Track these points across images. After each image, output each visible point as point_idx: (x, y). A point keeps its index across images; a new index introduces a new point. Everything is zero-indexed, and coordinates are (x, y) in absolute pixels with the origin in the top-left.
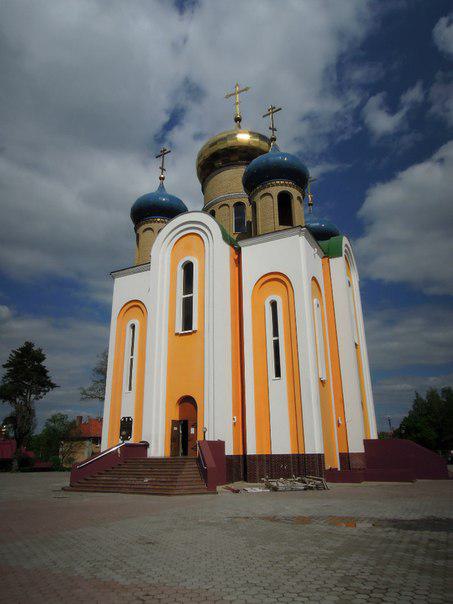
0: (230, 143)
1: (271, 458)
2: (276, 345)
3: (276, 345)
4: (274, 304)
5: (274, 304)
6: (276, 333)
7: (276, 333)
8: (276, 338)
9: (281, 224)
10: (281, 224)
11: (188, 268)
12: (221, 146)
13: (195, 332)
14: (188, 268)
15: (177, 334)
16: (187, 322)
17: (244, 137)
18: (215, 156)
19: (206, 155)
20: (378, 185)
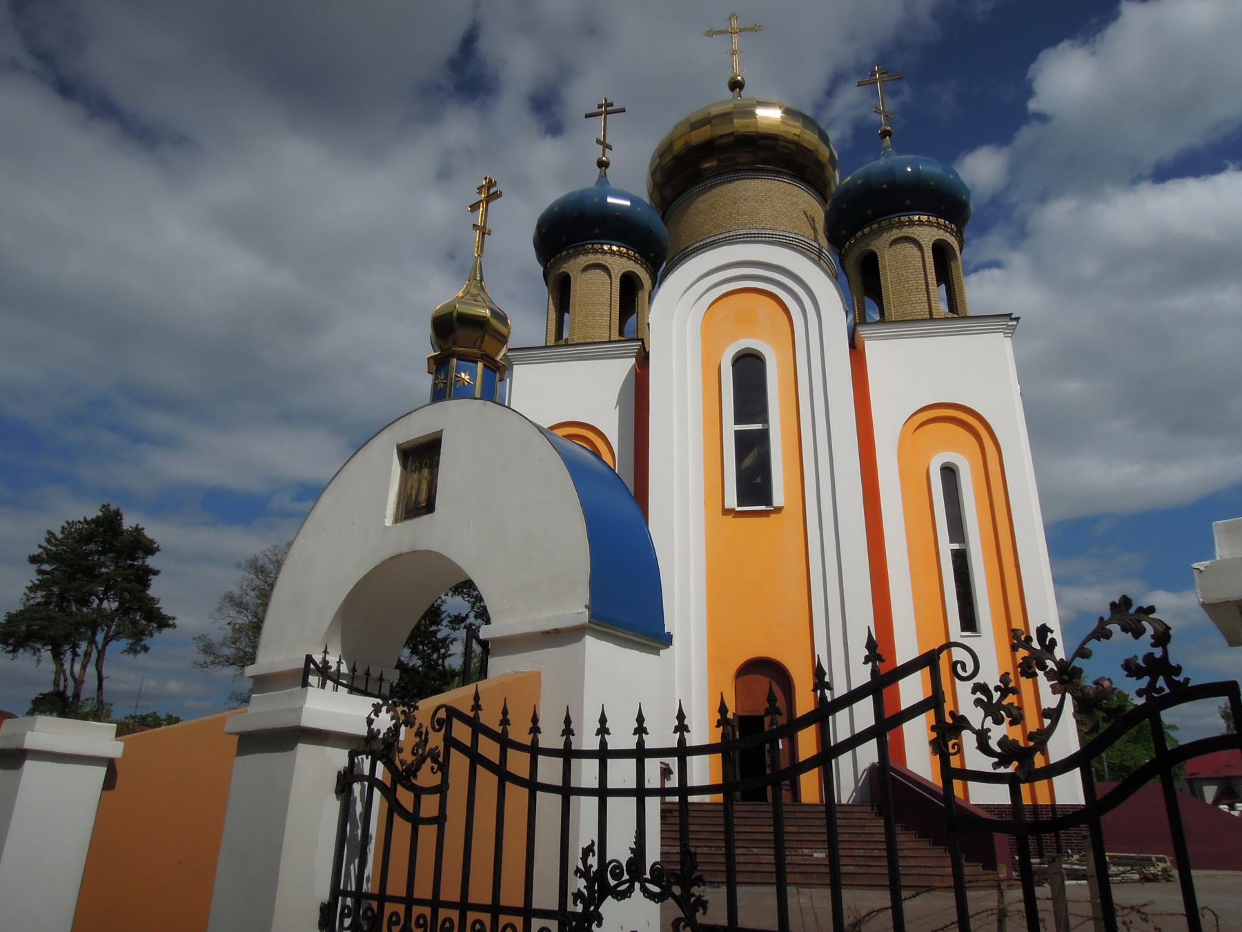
0: (739, 124)
1: (959, 921)
2: (961, 561)
3: (961, 561)
4: (949, 473)
5: (949, 473)
6: (957, 529)
7: (957, 529)
8: (956, 546)
9: (963, 629)
10: (963, 629)
11: (749, 368)
12: (722, 130)
13: (778, 510)
14: (749, 368)
15: (727, 512)
16: (754, 485)
17: (770, 115)
18: (708, 148)
19: (678, 146)
20: (1042, 55)
